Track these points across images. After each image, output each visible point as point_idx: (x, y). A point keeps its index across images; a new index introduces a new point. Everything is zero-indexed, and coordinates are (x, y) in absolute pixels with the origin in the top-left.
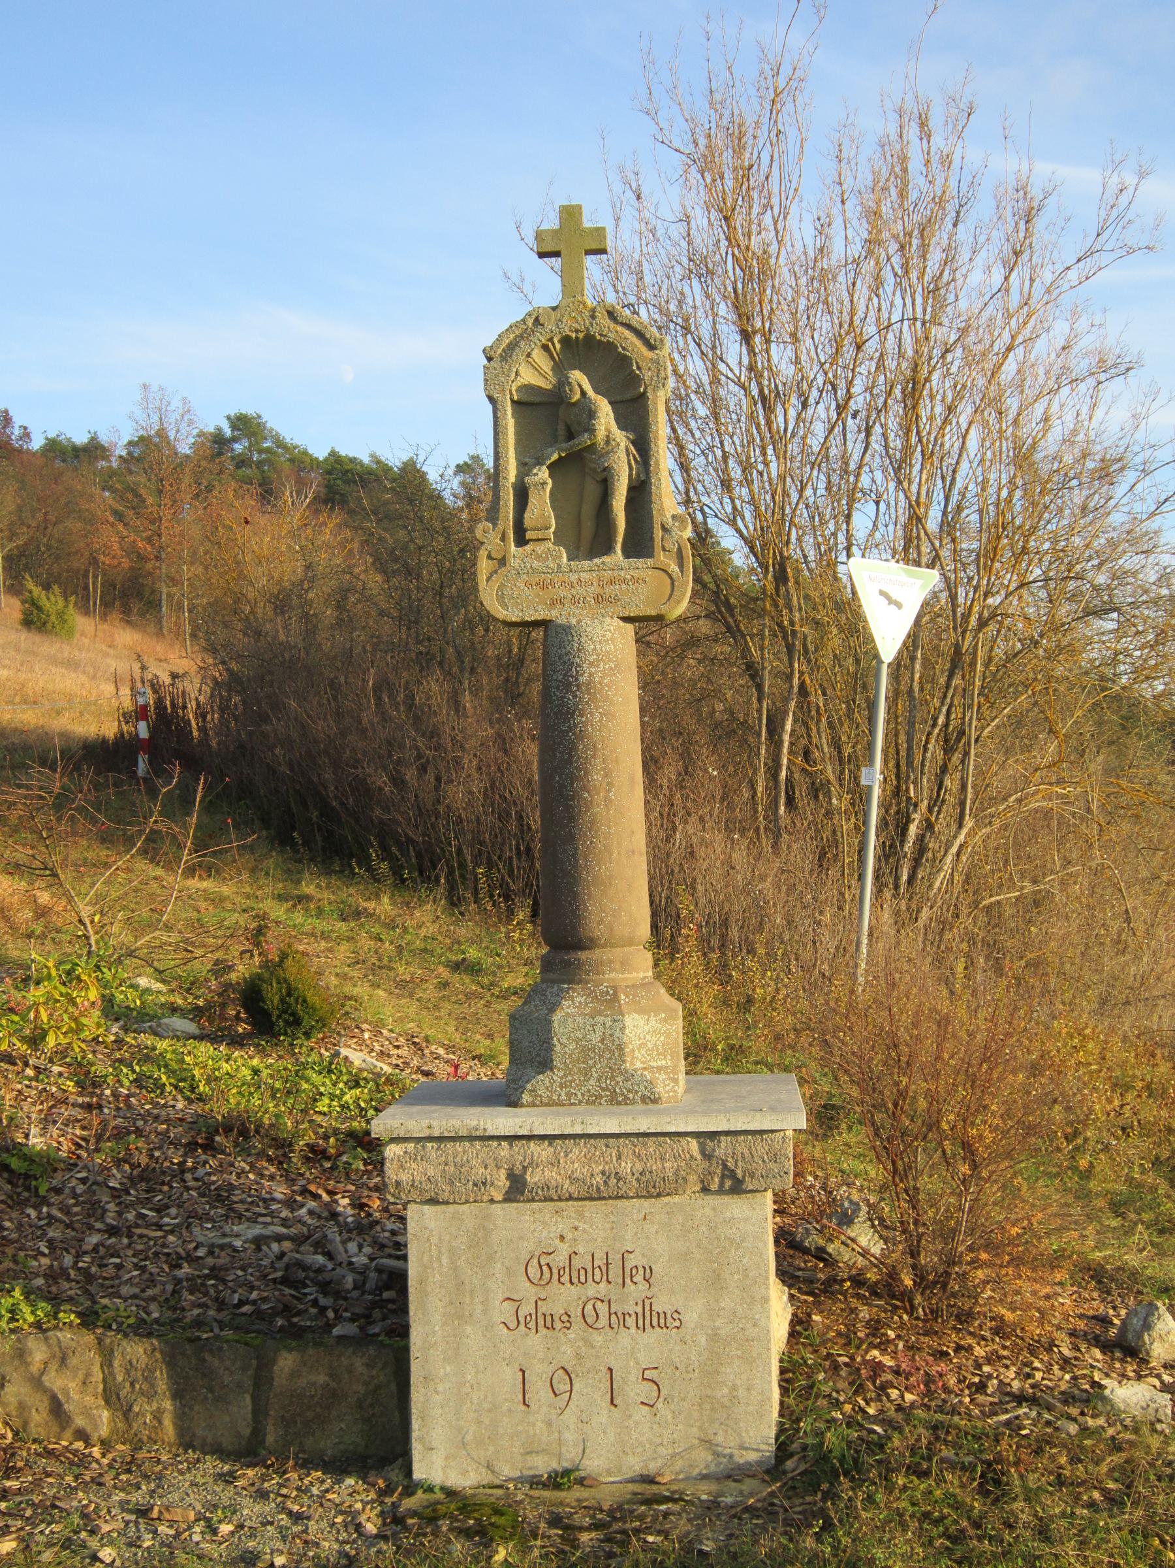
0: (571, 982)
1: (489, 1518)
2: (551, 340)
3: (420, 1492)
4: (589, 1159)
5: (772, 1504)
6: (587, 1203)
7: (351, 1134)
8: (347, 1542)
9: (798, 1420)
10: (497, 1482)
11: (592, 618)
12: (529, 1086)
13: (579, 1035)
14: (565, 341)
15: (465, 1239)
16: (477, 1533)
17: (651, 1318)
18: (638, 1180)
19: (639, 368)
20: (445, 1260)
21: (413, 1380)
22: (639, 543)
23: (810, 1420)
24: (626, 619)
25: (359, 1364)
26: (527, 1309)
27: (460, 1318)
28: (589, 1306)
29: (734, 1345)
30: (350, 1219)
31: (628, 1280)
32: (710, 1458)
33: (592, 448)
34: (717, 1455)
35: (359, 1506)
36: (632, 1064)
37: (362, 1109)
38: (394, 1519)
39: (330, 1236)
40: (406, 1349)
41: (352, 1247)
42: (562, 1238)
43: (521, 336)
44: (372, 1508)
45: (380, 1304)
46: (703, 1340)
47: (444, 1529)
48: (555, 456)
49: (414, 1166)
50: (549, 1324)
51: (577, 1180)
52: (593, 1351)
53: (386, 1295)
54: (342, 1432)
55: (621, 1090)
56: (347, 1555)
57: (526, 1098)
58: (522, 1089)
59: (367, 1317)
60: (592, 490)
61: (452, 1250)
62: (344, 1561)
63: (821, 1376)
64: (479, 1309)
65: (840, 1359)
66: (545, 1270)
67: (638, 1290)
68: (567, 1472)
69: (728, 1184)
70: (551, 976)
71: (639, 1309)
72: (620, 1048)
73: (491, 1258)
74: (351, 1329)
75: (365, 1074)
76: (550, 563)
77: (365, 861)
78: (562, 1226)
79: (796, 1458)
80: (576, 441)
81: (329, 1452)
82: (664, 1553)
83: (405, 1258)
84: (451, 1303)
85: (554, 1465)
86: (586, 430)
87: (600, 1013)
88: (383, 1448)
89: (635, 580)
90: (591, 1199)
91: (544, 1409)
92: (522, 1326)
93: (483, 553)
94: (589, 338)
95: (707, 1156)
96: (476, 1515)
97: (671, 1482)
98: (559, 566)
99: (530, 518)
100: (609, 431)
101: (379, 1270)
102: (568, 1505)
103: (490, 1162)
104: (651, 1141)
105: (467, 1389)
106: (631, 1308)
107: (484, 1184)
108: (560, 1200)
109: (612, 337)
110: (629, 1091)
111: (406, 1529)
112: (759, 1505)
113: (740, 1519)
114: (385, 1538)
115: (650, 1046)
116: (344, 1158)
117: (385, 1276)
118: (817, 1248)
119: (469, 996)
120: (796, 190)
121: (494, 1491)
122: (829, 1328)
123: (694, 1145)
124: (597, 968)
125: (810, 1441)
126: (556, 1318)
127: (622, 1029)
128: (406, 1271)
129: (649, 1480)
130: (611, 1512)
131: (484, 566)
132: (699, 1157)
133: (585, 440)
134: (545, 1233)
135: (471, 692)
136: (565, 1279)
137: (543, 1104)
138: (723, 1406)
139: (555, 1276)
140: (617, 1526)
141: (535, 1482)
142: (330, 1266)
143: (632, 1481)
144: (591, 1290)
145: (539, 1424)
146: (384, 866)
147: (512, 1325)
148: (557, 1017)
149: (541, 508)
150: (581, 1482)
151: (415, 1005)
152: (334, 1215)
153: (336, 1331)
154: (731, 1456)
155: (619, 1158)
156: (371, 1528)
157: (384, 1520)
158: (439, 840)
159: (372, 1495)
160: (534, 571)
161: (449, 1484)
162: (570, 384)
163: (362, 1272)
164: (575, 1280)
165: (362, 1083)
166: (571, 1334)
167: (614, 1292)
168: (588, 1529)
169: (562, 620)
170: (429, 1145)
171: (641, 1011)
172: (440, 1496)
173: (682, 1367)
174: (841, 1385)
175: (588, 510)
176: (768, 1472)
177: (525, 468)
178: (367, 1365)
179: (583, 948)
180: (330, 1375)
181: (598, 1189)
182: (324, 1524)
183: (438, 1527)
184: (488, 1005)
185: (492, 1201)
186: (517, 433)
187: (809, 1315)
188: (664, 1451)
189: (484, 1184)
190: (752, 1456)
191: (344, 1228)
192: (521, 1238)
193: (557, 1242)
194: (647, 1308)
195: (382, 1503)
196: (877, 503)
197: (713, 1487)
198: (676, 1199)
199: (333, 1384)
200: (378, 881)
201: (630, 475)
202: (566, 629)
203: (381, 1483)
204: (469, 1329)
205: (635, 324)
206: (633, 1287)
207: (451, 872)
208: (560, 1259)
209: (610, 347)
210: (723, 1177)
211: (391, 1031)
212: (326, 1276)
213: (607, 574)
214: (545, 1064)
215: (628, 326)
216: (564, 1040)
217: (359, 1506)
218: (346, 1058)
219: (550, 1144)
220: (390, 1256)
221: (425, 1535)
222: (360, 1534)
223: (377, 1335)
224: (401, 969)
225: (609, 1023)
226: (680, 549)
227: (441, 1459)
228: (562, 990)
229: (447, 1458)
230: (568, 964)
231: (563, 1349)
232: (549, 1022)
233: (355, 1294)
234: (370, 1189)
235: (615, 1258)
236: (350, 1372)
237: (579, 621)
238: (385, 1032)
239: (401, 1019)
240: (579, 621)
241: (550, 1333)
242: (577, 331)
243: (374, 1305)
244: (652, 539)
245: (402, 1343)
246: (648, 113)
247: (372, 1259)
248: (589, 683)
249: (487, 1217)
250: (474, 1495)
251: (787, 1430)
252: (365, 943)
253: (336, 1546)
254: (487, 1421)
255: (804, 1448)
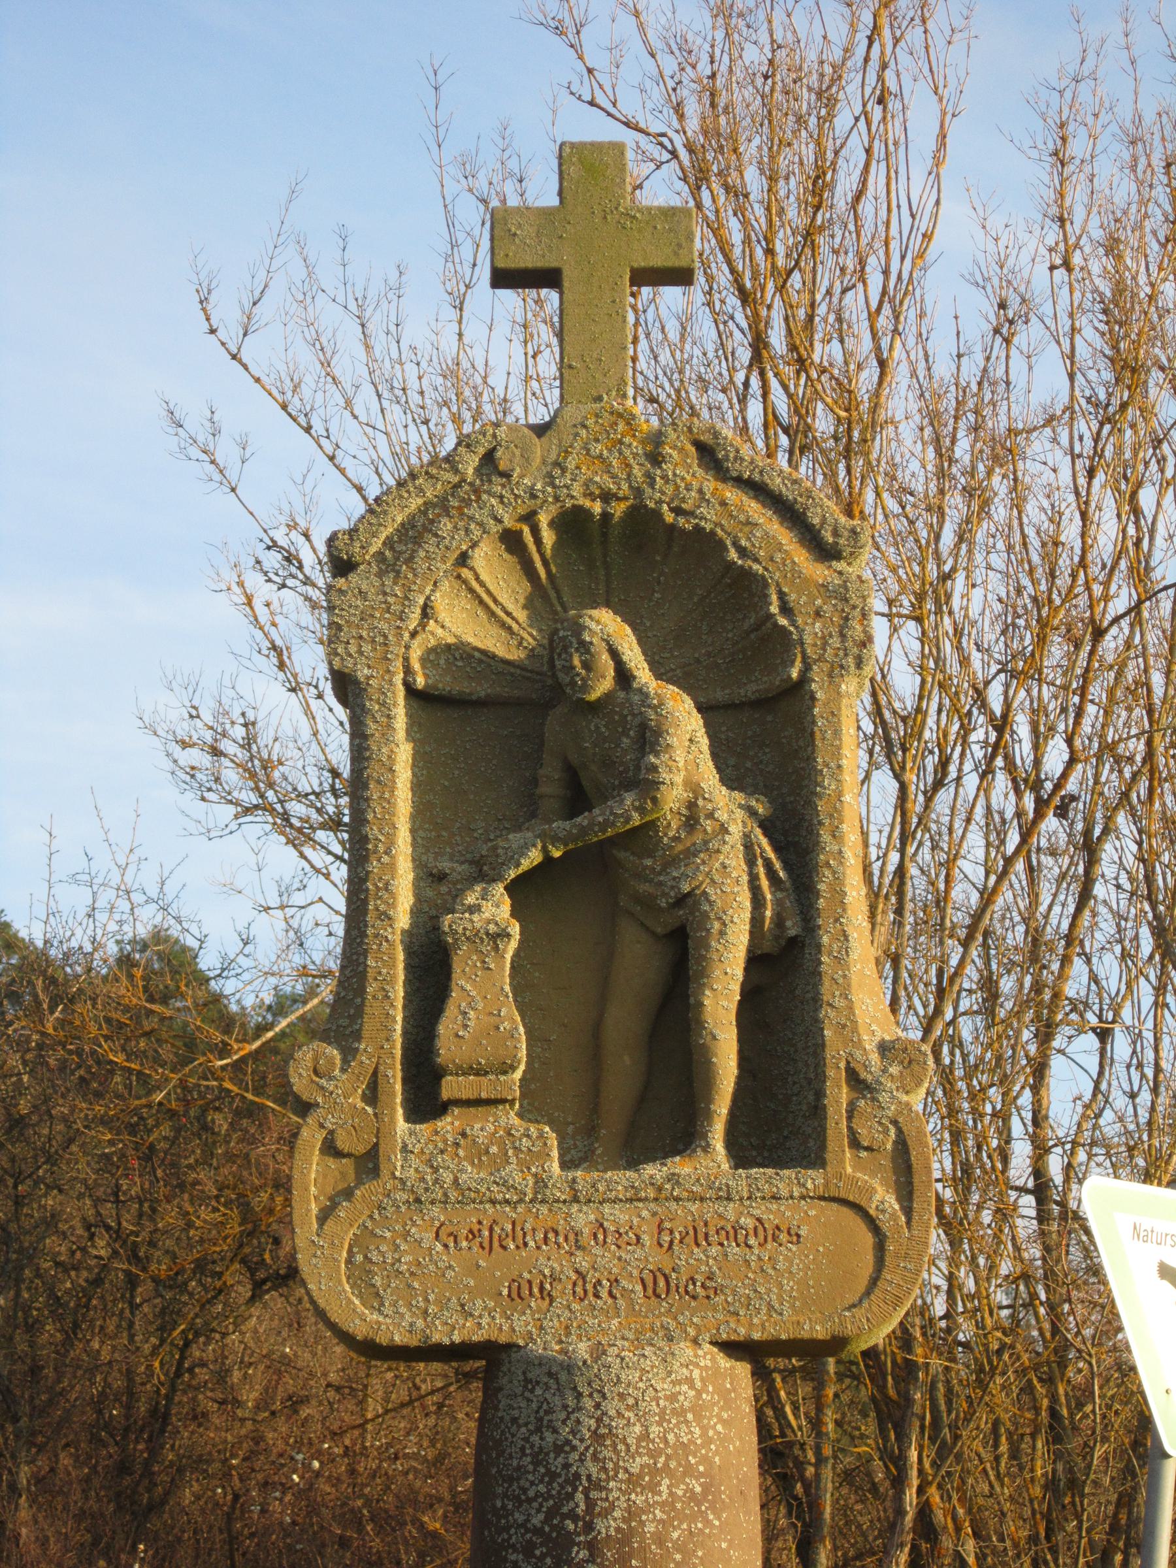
2: (530, 518)
11: (638, 1343)
14: (572, 523)
19: (786, 610)
22: (781, 1122)
24: (732, 1348)
33: (643, 837)
43: (442, 505)
48: (534, 857)
60: (638, 961)
76: (512, 1172)
80: (599, 816)
86: (631, 784)
89: (769, 1234)
93: (311, 1136)
94: (642, 518)
98: (540, 1183)
99: (454, 1036)
100: (695, 789)
109: (709, 517)
120: (927, 237)
131: (313, 1175)
133: (626, 810)
135: (33, 1501)
149: (486, 1010)
160: (466, 1196)
162: (585, 647)
169: (545, 1346)
175: (625, 1021)
177: (439, 888)
186: (418, 786)
196: (1104, 1035)
201: (756, 921)
202: (559, 1375)
205: (776, 483)
209: (705, 544)
213: (683, 1214)
215: (758, 489)
226: (902, 1146)
237: (599, 1351)
240: (599, 1351)
242: (607, 497)
244: (818, 1111)
246: (560, 31)
248: (625, 1538)
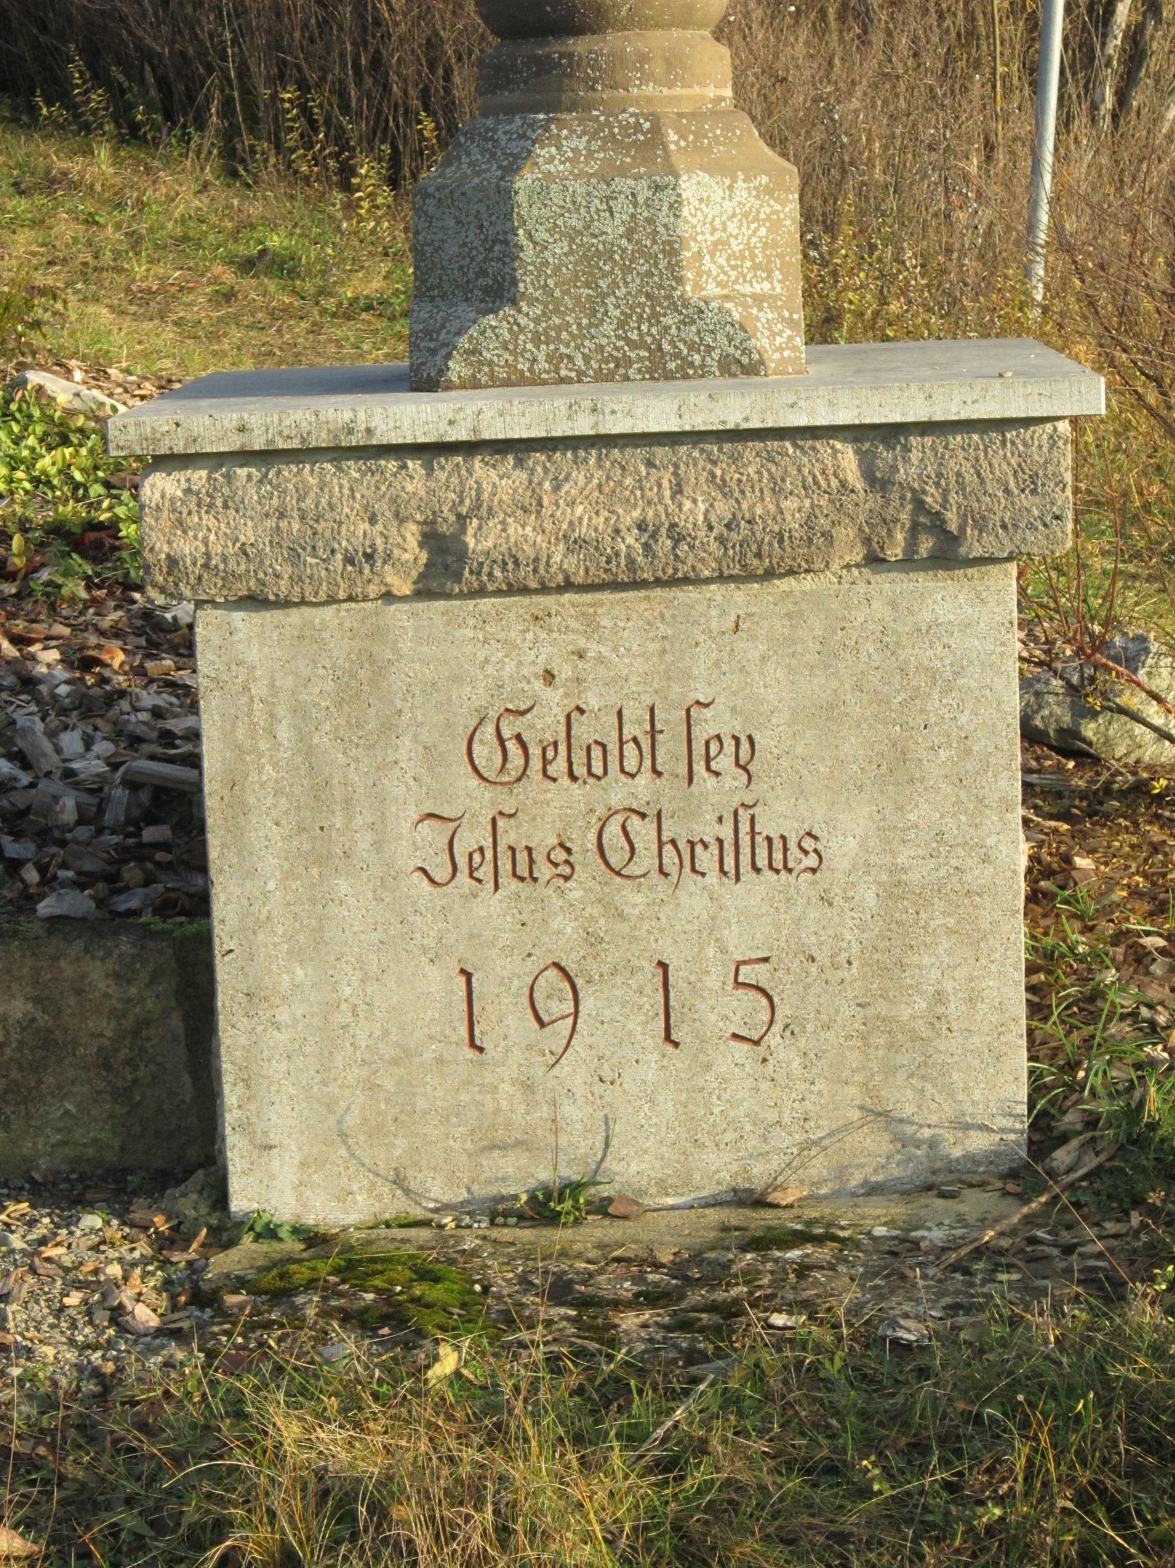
0: (552, 107)
1: (408, 1286)
3: (247, 1239)
4: (608, 497)
5: (1033, 1241)
6: (605, 596)
7: (57, 530)
8: (95, 1347)
9: (1072, 1066)
10: (418, 1213)
12: (464, 342)
13: (575, 222)
15: (328, 686)
16: (385, 1319)
17: (754, 851)
18: (721, 540)
20: (284, 733)
21: (223, 999)
23: (1098, 1064)
25: (98, 974)
26: (472, 837)
27: (321, 861)
28: (614, 828)
29: (940, 905)
30: (63, 690)
31: (699, 768)
32: (887, 1147)
34: (904, 1142)
35: (115, 1270)
36: (697, 286)
37: (76, 486)
38: (196, 1297)
39: (21, 720)
40: (206, 940)
41: (71, 741)
42: (549, 677)
44: (145, 1275)
45: (140, 853)
46: (868, 896)
47: (311, 1312)
49: (208, 520)
50: (523, 870)
51: (580, 543)
52: (624, 928)
53: (150, 834)
54: (70, 1120)
55: (675, 340)
56: (96, 1373)
57: (457, 368)
58: (448, 349)
59: (111, 878)
61: (299, 711)
62: (90, 1387)
63: (1111, 976)
64: (364, 841)
65: (1148, 941)
66: (512, 749)
67: (721, 789)
68: (575, 1188)
69: (926, 545)
70: (505, 97)
71: (727, 832)
72: (672, 250)
73: (389, 728)
74: (78, 903)
75: (80, 421)
77: (59, 92)
78: (548, 650)
79: (1074, 1143)
81: (43, 1163)
82: (818, 1348)
83: (194, 761)
84: (302, 829)
85: (543, 1174)
87: (623, 172)
88: (162, 1147)
90: (615, 586)
91: (517, 1055)
92: (463, 876)
95: (877, 482)
96: (378, 1282)
97: (802, 1202)
101: (133, 784)
102: (579, 1256)
103: (382, 507)
104: (750, 451)
105: (343, 1016)
106: (708, 830)
107: (369, 557)
108: (544, 589)
110: (692, 347)
111: (224, 1314)
112: (1005, 1243)
113: (967, 1272)
114: (178, 1335)
115: (736, 246)
116: (44, 575)
117: (144, 796)
118: (1061, 731)
119: (278, 315)
121: (412, 1233)
122: (1111, 883)
123: (848, 458)
124: (613, 73)
125: (1104, 1107)
126: (539, 857)
127: (675, 207)
128: (198, 787)
129: (760, 1202)
130: (678, 1269)
132: (859, 485)
134: (510, 666)
136: (559, 767)
137: (495, 382)
138: (916, 1038)
139: (536, 763)
140: (696, 1297)
141: (499, 1212)
142: (25, 779)
143: (715, 1203)
144: (618, 792)
145: (506, 1087)
146: (97, 98)
147: (441, 875)
148: (525, 181)
150: (603, 1208)
151: (169, 333)
152: (28, 683)
153: (45, 907)
154: (933, 1144)
155: (678, 490)
156: (145, 1316)
157: (173, 1298)
158: (202, 53)
159: (143, 1248)
161: (310, 1220)
163: (97, 789)
164: (580, 770)
165: (74, 438)
166: (574, 889)
167: (668, 793)
168: (634, 1304)
170: (242, 472)
171: (715, 169)
172: (293, 1246)
173: (822, 957)
174: (1155, 993)
176: (1012, 1174)
178: (116, 976)
179: (578, 31)
180: (37, 1000)
181: (631, 561)
182: (40, 1310)
183: (296, 1309)
184: (315, 329)
185: (388, 597)
187: (1067, 859)
188: (786, 1140)
189: (369, 557)
190: (979, 1143)
191: (49, 706)
192: (456, 679)
193: (538, 685)
194: (744, 828)
195: (165, 1263)
197: (899, 1210)
198: (807, 583)
199: (44, 1020)
200: (86, 127)
203: (161, 1223)
204: (343, 886)
206: (711, 781)
207: (228, 102)
208: (546, 723)
210: (915, 530)
211: (128, 372)
212: (20, 800)
214: (499, 292)
216: (542, 235)
217: (115, 1270)
218: (40, 389)
219: (520, 463)
220: (152, 757)
221: (268, 1325)
222: (123, 1329)
223: (136, 913)
224: (140, 270)
225: (644, 194)
227: (291, 1165)
228: (532, 125)
229: (303, 1165)
230: (545, 66)
231: (555, 925)
232: (504, 195)
233: (83, 832)
234: (102, 633)
235: (671, 719)
236: (79, 992)
238: (112, 371)
239: (146, 355)
241: (525, 889)
243: (125, 855)
245: (192, 928)
247: (114, 766)
249: (377, 634)
250: (369, 1243)
251: (1048, 1088)
252: (65, 229)
253: (71, 1355)
254: (389, 1084)
255: (1092, 1122)
